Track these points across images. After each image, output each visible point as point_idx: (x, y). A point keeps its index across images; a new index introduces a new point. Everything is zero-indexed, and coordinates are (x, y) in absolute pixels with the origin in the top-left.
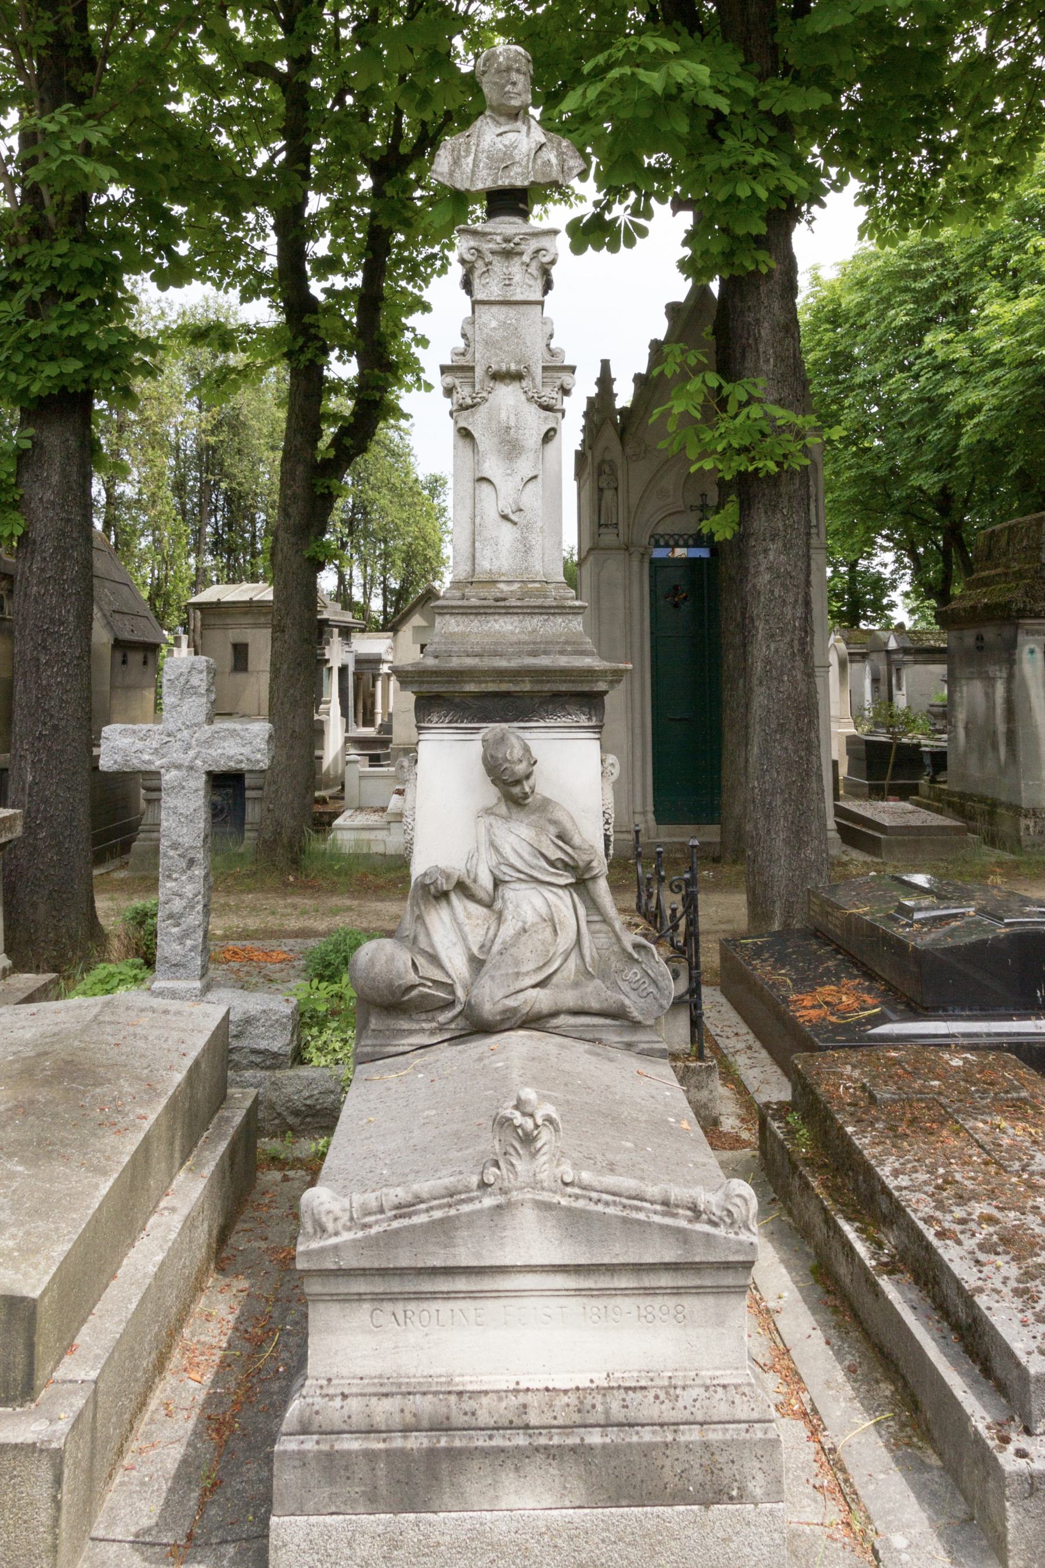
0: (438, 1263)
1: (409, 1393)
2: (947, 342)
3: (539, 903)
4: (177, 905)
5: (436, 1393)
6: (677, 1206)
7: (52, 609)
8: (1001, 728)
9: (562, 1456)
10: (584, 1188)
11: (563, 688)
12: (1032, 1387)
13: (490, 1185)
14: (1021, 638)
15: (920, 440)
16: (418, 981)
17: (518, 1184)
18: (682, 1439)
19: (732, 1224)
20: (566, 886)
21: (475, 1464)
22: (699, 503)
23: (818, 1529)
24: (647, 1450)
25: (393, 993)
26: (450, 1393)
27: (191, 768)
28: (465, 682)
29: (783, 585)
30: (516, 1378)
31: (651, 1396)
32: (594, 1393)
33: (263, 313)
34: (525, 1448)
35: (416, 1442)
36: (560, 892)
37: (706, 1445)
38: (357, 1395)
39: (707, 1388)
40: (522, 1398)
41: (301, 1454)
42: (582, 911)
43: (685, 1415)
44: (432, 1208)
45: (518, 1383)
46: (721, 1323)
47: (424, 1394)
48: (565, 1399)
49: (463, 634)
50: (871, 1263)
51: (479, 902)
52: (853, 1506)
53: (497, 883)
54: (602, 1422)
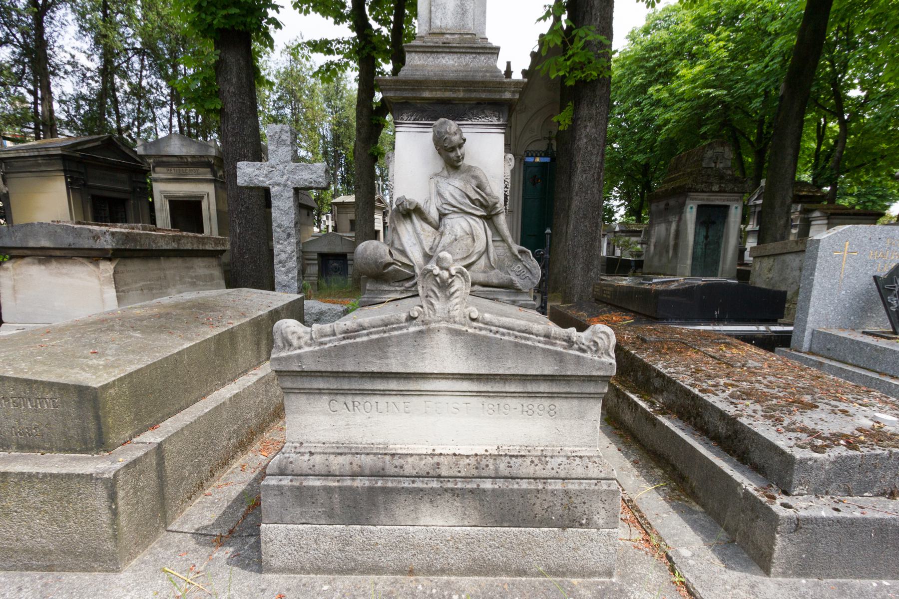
0: (375, 369)
1: (357, 454)
2: (658, 91)
3: (465, 225)
4: (283, 256)
5: (375, 454)
6: (556, 338)
7: (240, 149)
8: (672, 243)
9: (463, 495)
10: (486, 324)
11: (484, 96)
12: (796, 467)
13: (415, 318)
14: (688, 202)
15: (641, 139)
16: (392, 261)
17: (436, 318)
18: (549, 488)
19: (596, 351)
20: (480, 217)
21: (402, 498)
22: (548, 136)
23: (628, 543)
24: (524, 494)
25: (378, 267)
26: (386, 454)
27: (285, 185)
28: (424, 90)
29: (593, 145)
30: (433, 447)
31: (528, 461)
32: (488, 458)
33: (345, 32)
34: (438, 489)
35: (360, 483)
36: (477, 219)
37: (566, 492)
38: (320, 453)
39: (568, 458)
40: (436, 459)
41: (279, 488)
42: (489, 233)
43: (553, 473)
44: (371, 333)
45: (434, 450)
46: (581, 417)
47: (368, 454)
48: (468, 461)
49: (423, 66)
50: (650, 410)
51: (430, 223)
52: (648, 531)
53: (442, 216)
54: (493, 476)
